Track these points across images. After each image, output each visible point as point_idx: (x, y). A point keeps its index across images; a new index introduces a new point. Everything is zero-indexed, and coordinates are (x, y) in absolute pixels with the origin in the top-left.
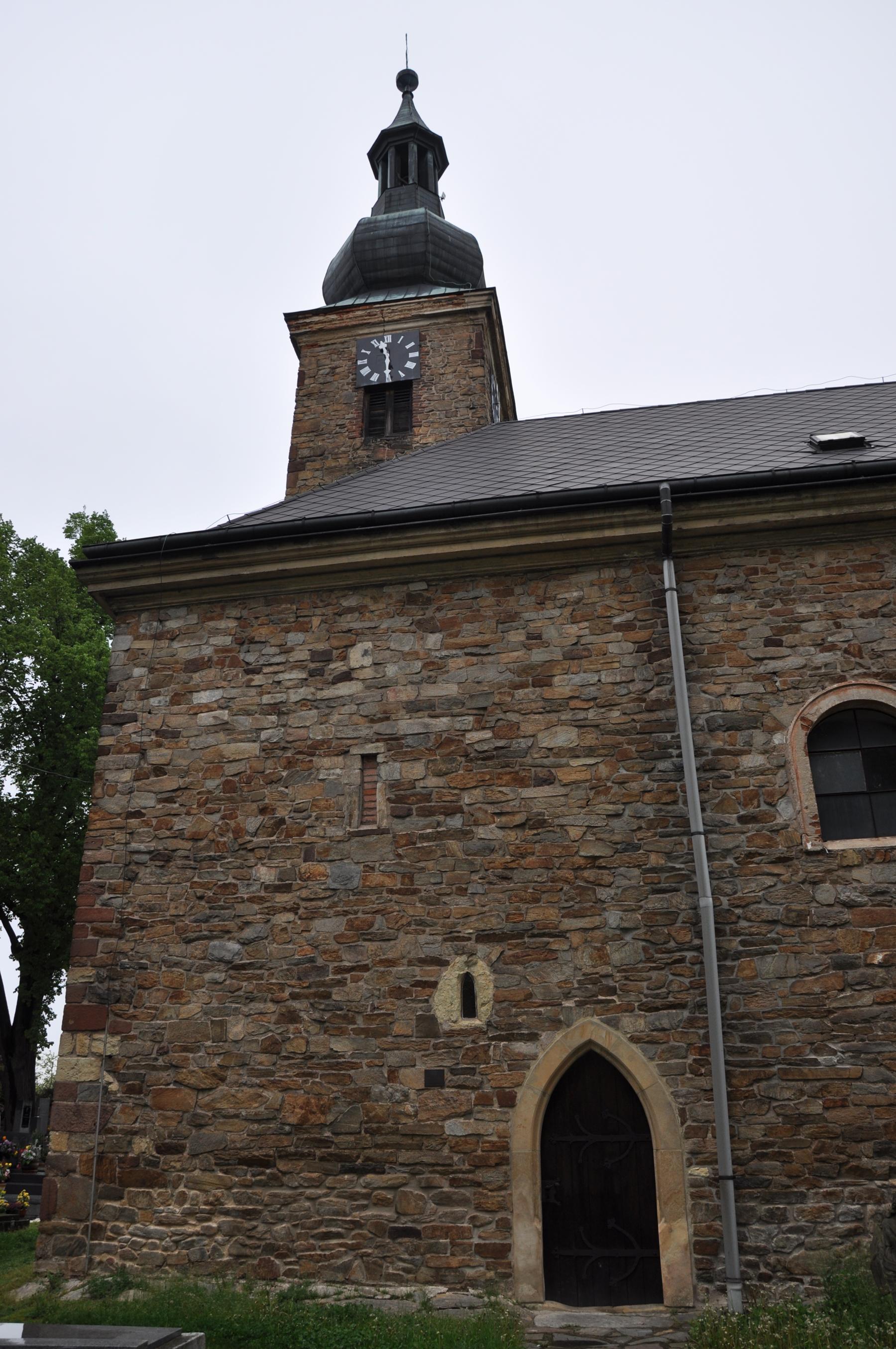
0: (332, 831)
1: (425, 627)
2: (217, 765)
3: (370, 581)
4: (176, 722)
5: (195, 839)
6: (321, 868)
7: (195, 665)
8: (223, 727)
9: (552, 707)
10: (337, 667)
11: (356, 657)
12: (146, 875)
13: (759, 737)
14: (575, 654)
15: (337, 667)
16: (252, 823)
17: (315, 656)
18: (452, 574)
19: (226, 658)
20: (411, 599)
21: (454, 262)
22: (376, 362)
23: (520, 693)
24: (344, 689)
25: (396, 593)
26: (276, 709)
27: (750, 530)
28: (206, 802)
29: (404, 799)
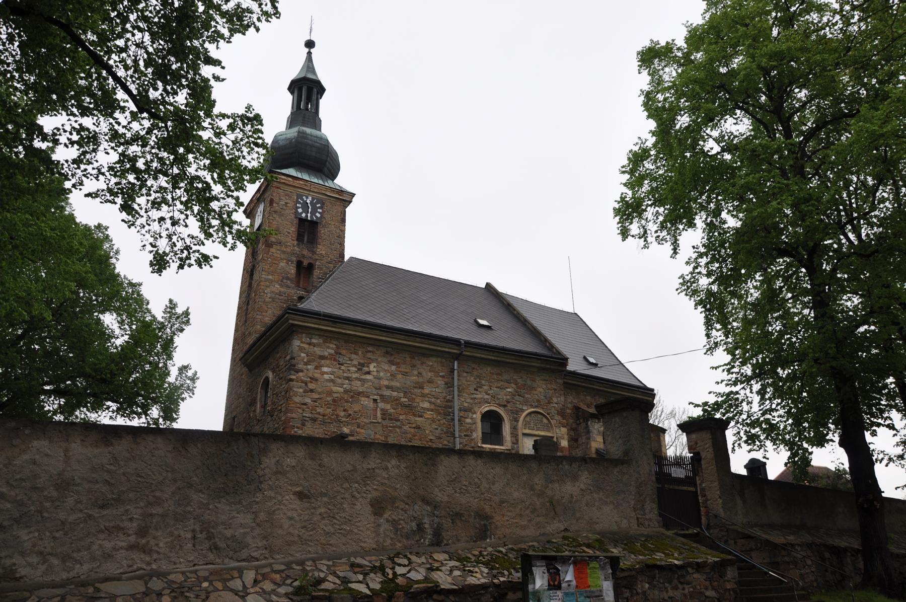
0: (365, 420)
1: (391, 363)
2: (330, 393)
3: (377, 344)
4: (317, 375)
5: (324, 416)
6: (363, 431)
7: (322, 358)
8: (332, 381)
9: (423, 395)
10: (366, 369)
11: (372, 367)
12: (308, 425)
13: (470, 415)
14: (430, 381)
15: (366, 369)
16: (342, 414)
17: (360, 364)
18: (400, 349)
19: (332, 358)
20: (387, 353)
21: (324, 161)
22: (305, 206)
23: (416, 390)
24: (368, 377)
25: (384, 350)
26: (348, 378)
27: (476, 357)
28: (328, 405)
29: (384, 413)
